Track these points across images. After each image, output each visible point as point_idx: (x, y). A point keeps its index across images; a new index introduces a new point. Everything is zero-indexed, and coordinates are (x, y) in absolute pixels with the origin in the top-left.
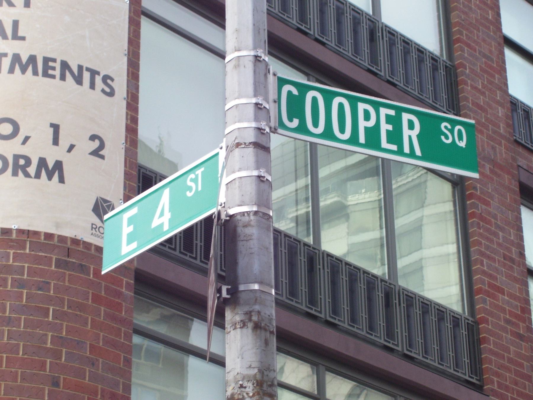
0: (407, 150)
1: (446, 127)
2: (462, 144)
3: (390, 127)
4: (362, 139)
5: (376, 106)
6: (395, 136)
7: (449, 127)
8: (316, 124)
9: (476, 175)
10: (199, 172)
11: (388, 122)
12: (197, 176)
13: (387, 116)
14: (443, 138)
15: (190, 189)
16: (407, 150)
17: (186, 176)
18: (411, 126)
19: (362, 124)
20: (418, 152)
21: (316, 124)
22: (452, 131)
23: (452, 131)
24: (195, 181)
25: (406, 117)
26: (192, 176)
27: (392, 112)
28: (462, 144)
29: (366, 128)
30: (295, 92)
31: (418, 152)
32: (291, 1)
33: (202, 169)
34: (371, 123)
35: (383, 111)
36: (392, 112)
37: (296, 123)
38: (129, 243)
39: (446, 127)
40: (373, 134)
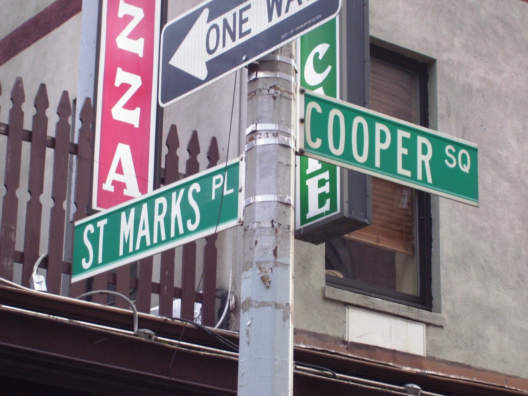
0: (420, 177)
1: (450, 151)
2: (466, 169)
3: (405, 151)
5: (394, 127)
6: (410, 162)
9: (213, 198)
11: (404, 146)
13: (404, 139)
14: (446, 161)
16: (420, 177)
18: (425, 152)
19: (379, 146)
20: (430, 180)
22: (456, 155)
23: (456, 155)
25: (421, 140)
27: (408, 135)
28: (466, 169)
29: (381, 151)
30: (319, 110)
31: (430, 180)
32: (2, 286)
34: (386, 146)
35: (401, 134)
37: (318, 143)
39: (450, 151)
40: (389, 156)
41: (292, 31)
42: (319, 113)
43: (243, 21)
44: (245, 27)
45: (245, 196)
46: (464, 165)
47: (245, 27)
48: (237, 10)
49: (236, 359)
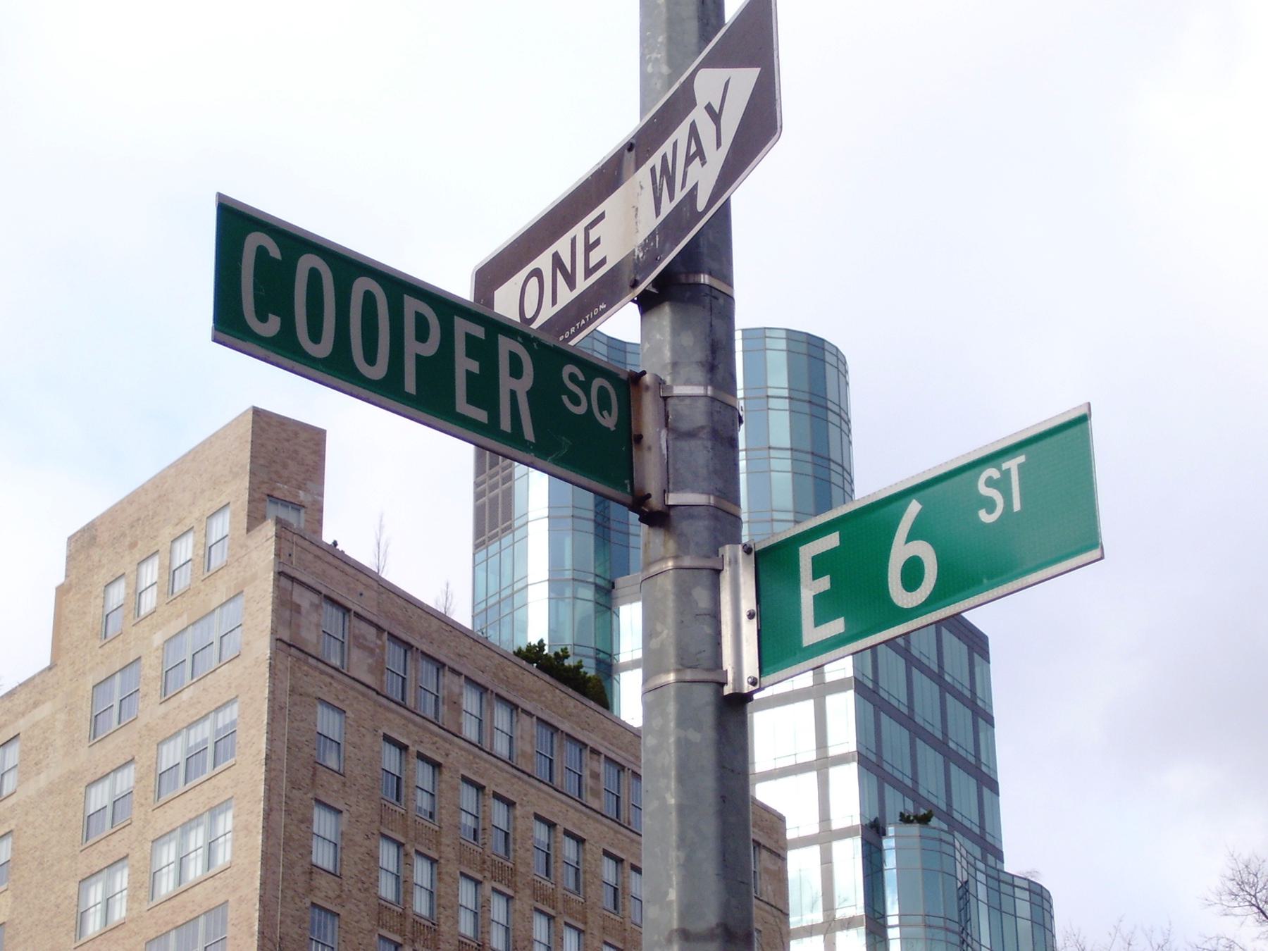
0: (506, 424)
1: (573, 377)
3: (474, 366)
4: (410, 386)
7: (582, 378)
10: (1013, 464)
11: (470, 354)
12: (1006, 474)
13: (469, 338)
14: (565, 398)
15: (990, 505)
16: (506, 424)
17: (976, 470)
18: (516, 372)
19: (412, 348)
20: (529, 434)
22: (586, 387)
23: (586, 387)
24: (1002, 484)
25: (506, 345)
26: (992, 472)
27: (479, 332)
28: (609, 421)
29: (419, 358)
30: (275, 252)
31: (529, 434)
33: (1021, 459)
34: (430, 348)
36: (479, 332)
37: (272, 326)
39: (573, 377)
41: (573, 330)
43: (589, 247)
44: (595, 257)
46: (605, 413)
47: (595, 257)
48: (578, 230)
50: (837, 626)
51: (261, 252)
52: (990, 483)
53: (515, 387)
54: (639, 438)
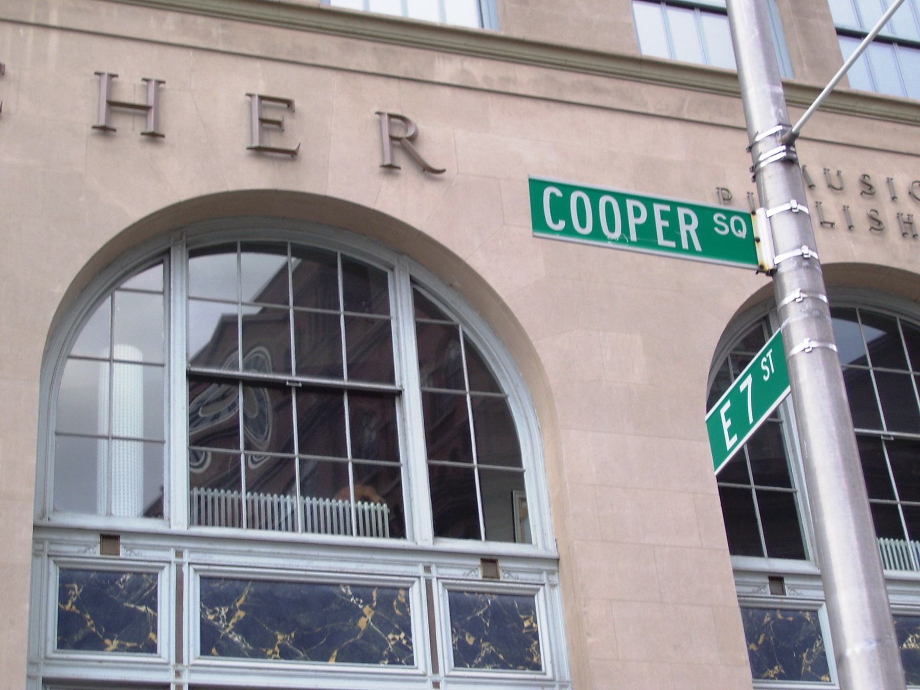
0: (685, 245)
1: (719, 219)
2: (742, 234)
3: (666, 224)
8: (583, 224)
10: (769, 354)
12: (768, 359)
14: (716, 229)
16: (685, 245)
18: (688, 220)
19: (632, 222)
20: (698, 247)
21: (583, 224)
22: (728, 223)
24: (767, 363)
25: (681, 212)
26: (764, 360)
27: (667, 208)
28: (742, 234)
29: (636, 225)
30: (559, 193)
31: (698, 247)
33: (771, 351)
36: (667, 208)
37: (562, 225)
38: (730, 439)
39: (719, 219)
42: (559, 198)
45: (779, 438)
49: (739, 579)
50: (735, 438)
51: (552, 195)
52: (764, 364)
53: (689, 229)
54: (758, 240)
